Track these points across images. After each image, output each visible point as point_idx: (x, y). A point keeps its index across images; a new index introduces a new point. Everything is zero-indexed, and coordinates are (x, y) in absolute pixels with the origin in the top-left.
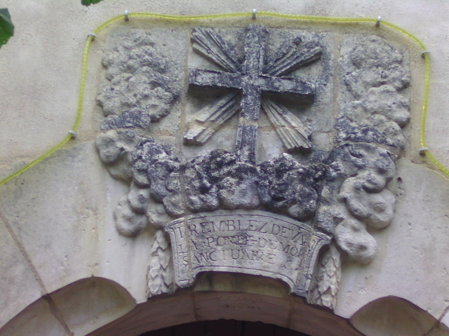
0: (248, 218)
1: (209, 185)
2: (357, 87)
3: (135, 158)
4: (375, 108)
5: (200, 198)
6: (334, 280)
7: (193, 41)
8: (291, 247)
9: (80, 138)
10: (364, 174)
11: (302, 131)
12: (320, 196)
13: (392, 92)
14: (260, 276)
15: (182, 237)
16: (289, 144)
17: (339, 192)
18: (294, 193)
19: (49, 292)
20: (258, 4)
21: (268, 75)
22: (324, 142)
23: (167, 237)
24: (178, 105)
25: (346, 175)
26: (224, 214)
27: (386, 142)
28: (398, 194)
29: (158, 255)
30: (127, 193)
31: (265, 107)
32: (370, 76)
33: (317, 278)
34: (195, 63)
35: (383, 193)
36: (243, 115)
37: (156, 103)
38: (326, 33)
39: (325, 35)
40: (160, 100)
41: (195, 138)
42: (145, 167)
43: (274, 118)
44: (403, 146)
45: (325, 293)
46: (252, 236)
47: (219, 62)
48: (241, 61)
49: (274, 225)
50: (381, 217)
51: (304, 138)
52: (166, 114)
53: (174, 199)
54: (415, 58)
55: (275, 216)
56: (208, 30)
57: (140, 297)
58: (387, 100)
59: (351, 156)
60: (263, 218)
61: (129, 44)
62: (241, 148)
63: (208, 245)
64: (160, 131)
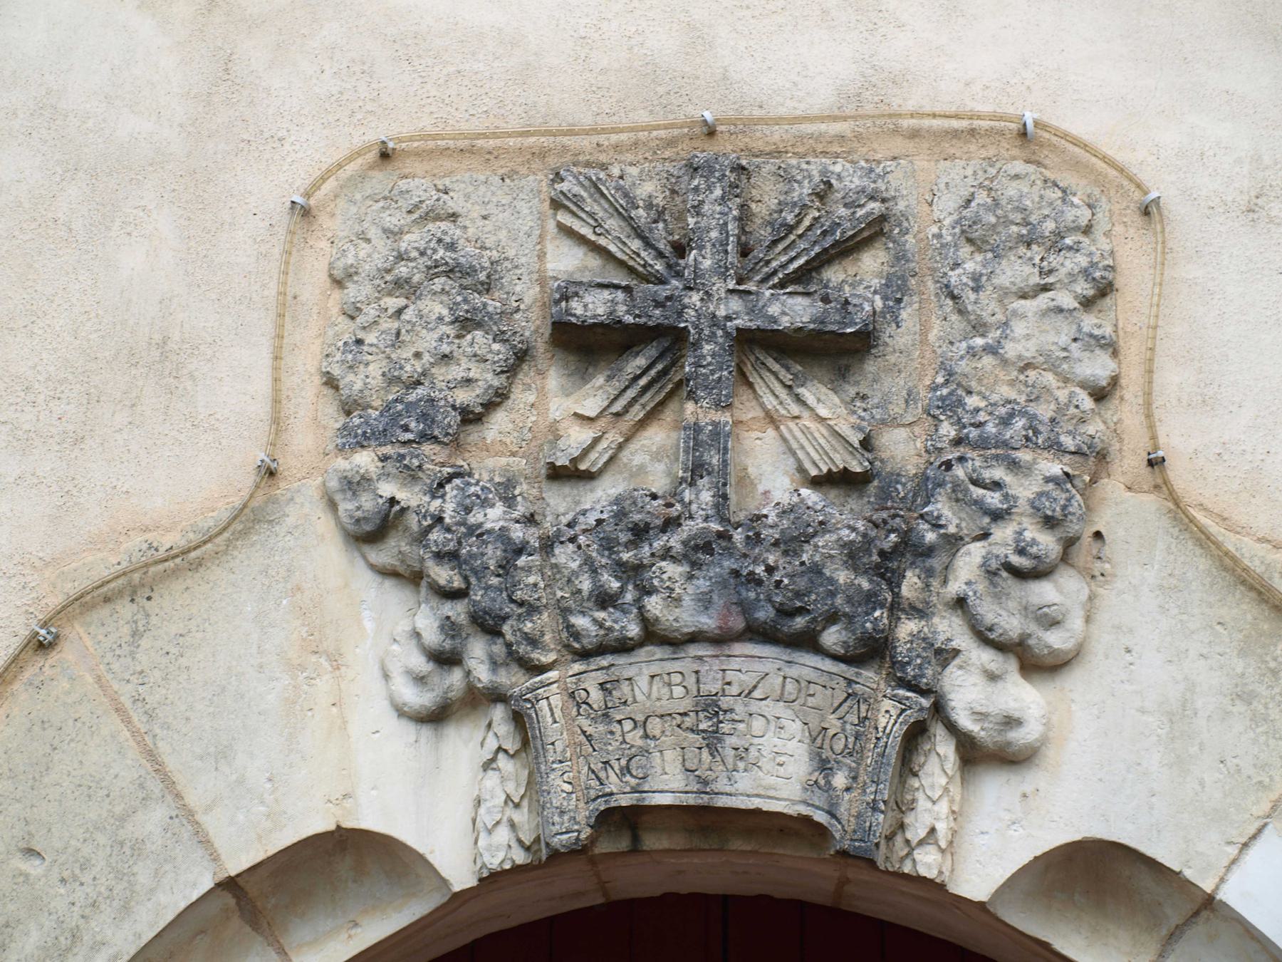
0: (716, 665)
1: (615, 585)
2: (986, 305)
3: (425, 523)
4: (1028, 354)
5: (595, 621)
6: (943, 807)
7: (556, 205)
8: (831, 732)
9: (286, 473)
10: (1003, 534)
11: (844, 429)
12: (897, 595)
13: (1071, 311)
14: (757, 812)
15: (555, 722)
16: (815, 463)
17: (945, 582)
18: (832, 594)
19: (233, 873)
20: (718, 96)
21: (750, 286)
22: (903, 449)
23: (519, 720)
24: (527, 375)
25: (962, 538)
26: (658, 656)
27: (1059, 444)
28: (1097, 574)
29: (498, 769)
30: (412, 612)
31: (748, 369)
32: (1016, 270)
33: (902, 806)
34: (566, 261)
35: (1056, 576)
36: (691, 396)
37: (471, 369)
38: (894, 163)
39: (893, 168)
40: (482, 365)
41: (574, 461)
42: (451, 546)
43: (772, 398)
44: (1103, 449)
45: (921, 843)
46: (732, 711)
47: (625, 258)
48: (680, 250)
49: (785, 678)
50: (1056, 640)
51: (851, 445)
52: (499, 400)
53: (529, 625)
54: (1125, 216)
55: (785, 654)
56: (592, 173)
57: (461, 878)
58: (1058, 333)
59: (972, 487)
60: (754, 664)
61: (394, 219)
62: (692, 484)
63: (621, 739)
64: (486, 445)
